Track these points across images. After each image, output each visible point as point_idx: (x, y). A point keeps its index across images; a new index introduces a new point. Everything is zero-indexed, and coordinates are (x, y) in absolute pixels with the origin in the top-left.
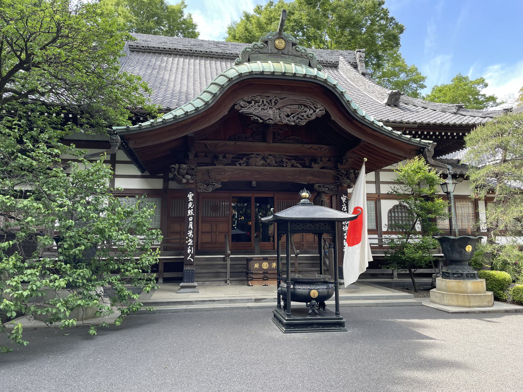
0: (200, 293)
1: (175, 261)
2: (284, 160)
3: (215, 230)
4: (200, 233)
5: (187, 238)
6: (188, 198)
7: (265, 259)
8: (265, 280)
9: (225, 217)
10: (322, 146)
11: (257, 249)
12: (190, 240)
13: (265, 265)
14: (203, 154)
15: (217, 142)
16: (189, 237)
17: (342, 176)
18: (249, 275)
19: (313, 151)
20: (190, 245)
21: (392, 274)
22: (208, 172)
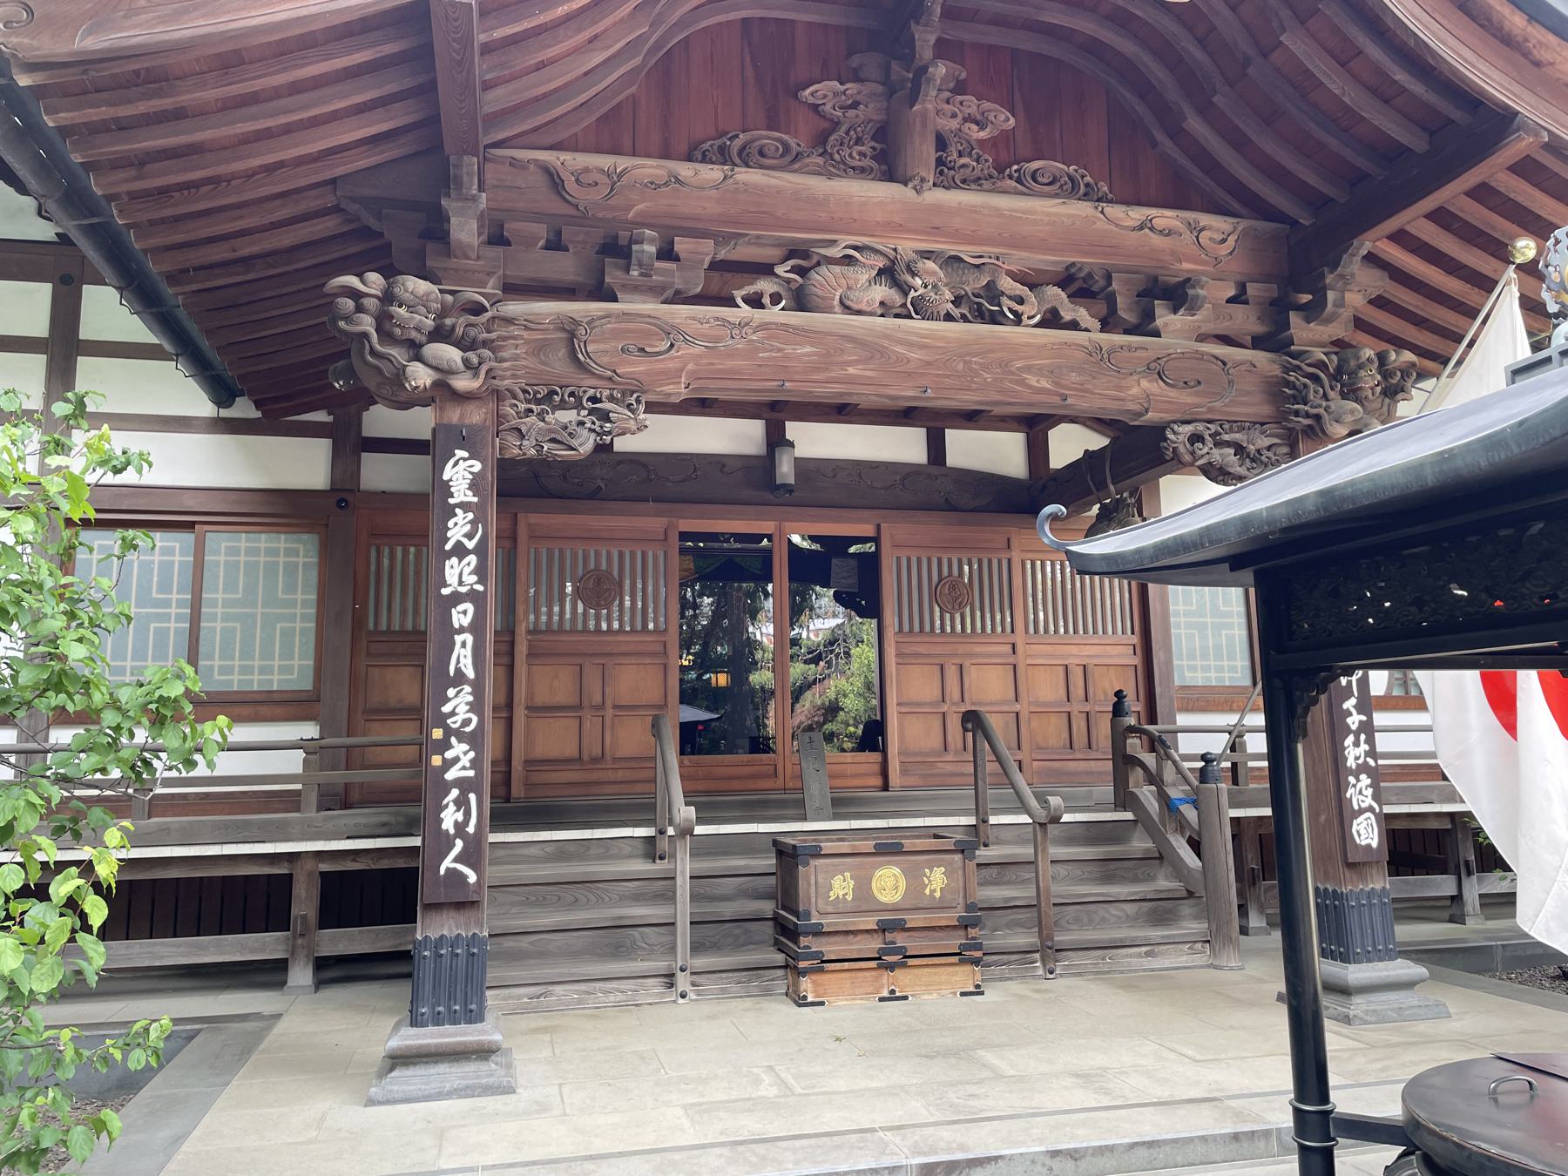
0: (524, 1095)
1: (385, 864)
2: (1007, 284)
3: (597, 699)
4: (520, 714)
5: (438, 734)
6: (446, 486)
7: (889, 849)
8: (891, 967)
9: (633, 631)
10: (1205, 219)
11: (817, 790)
12: (458, 749)
13: (889, 883)
14: (541, 231)
15: (623, 162)
16: (449, 732)
17: (1315, 379)
18: (804, 941)
19: (1156, 240)
20: (460, 783)
21: (1457, 899)
22: (572, 335)
